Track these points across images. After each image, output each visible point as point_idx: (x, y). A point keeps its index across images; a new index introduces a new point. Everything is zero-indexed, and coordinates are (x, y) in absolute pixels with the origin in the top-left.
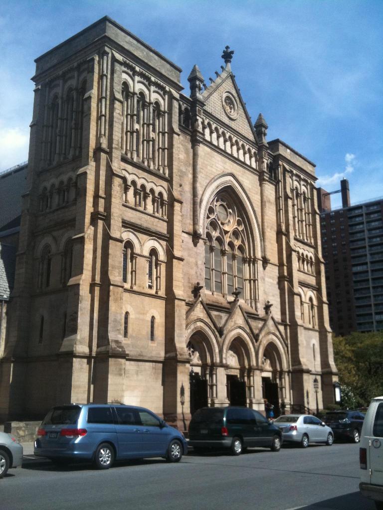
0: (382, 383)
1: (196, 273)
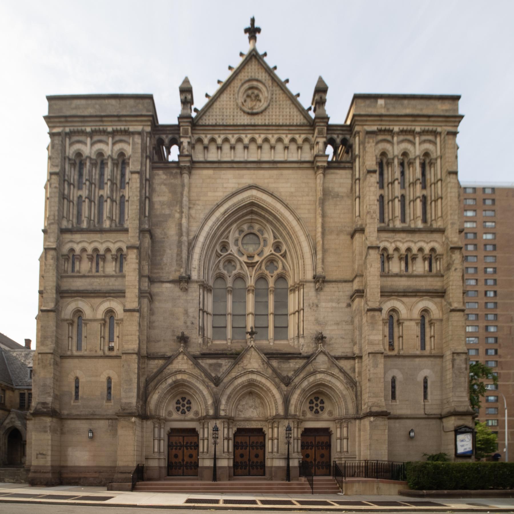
1: (185, 323)
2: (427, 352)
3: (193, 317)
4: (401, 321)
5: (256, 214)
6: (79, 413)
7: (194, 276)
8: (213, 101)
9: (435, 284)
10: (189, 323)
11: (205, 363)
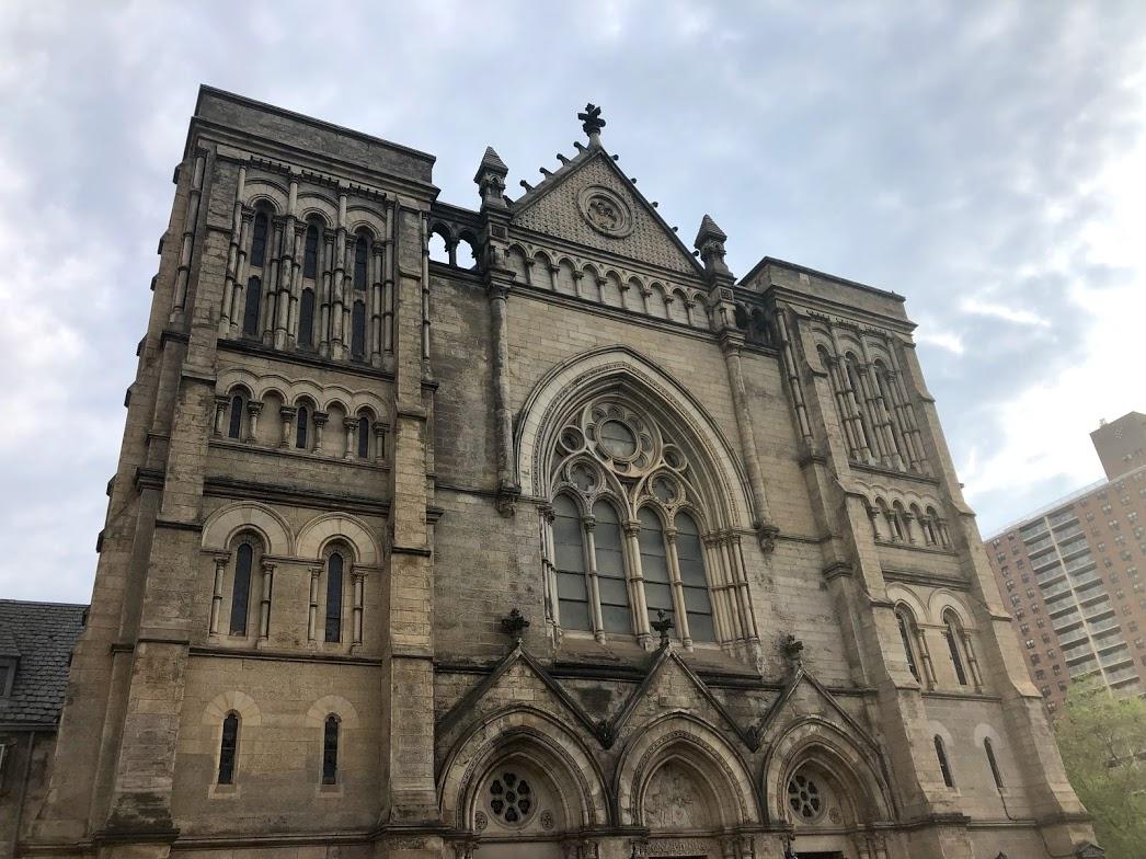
0: (736, 838)
1: (514, 587)
2: (341, 650)
3: (531, 576)
4: (919, 628)
5: (626, 391)
6: (231, 826)
7: (527, 488)
8: (535, 195)
9: (360, 484)
10: (522, 590)
11: (573, 687)
